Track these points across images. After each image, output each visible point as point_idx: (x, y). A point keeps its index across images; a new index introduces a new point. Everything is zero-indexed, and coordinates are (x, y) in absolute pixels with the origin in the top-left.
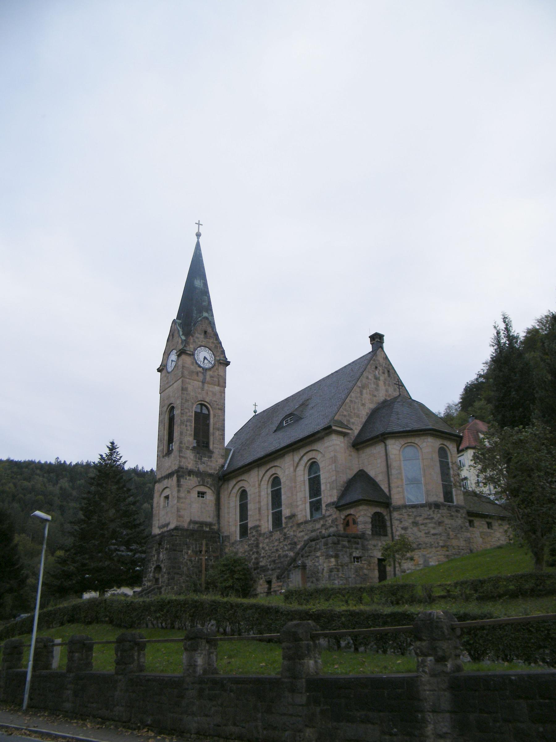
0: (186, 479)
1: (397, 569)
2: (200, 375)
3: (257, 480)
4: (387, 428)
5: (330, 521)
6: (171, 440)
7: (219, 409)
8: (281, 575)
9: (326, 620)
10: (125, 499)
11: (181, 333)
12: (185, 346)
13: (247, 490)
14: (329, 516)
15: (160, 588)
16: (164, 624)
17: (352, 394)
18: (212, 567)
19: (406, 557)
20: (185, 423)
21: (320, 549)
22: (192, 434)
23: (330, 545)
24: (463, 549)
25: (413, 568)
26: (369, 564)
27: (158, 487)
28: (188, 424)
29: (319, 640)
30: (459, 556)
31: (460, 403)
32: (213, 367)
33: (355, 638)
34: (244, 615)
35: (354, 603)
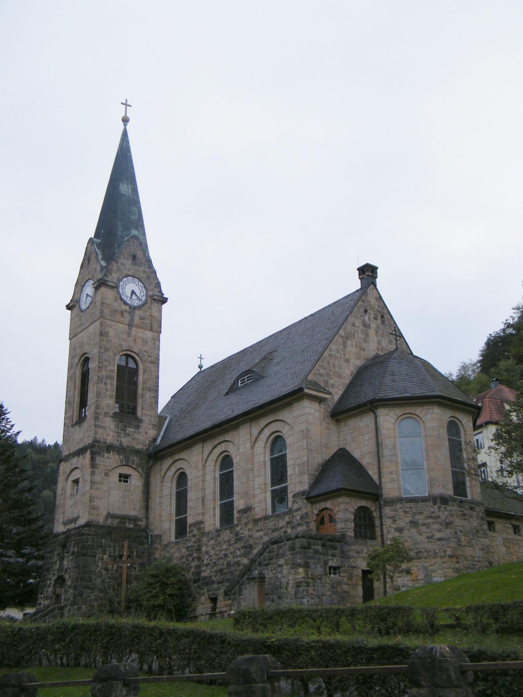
0: (103, 457)
1: (388, 585)
2: (126, 315)
3: (201, 459)
4: (378, 393)
5: (298, 517)
6: (83, 403)
7: (151, 362)
8: (230, 592)
9: (289, 654)
10: (16, 485)
11: (100, 257)
12: (105, 275)
13: (187, 472)
14: (297, 510)
15: (61, 609)
16: (64, 660)
17: (332, 346)
18: (137, 578)
19: (400, 569)
20: (104, 380)
21: (284, 555)
22: (113, 396)
23: (298, 550)
24: (478, 562)
25: (410, 584)
26: (350, 577)
27: (64, 467)
28: (108, 381)
29: (279, 681)
30: (474, 571)
31: (480, 361)
32: (143, 305)
33: (329, 679)
34: (177, 645)
35: (329, 630)
